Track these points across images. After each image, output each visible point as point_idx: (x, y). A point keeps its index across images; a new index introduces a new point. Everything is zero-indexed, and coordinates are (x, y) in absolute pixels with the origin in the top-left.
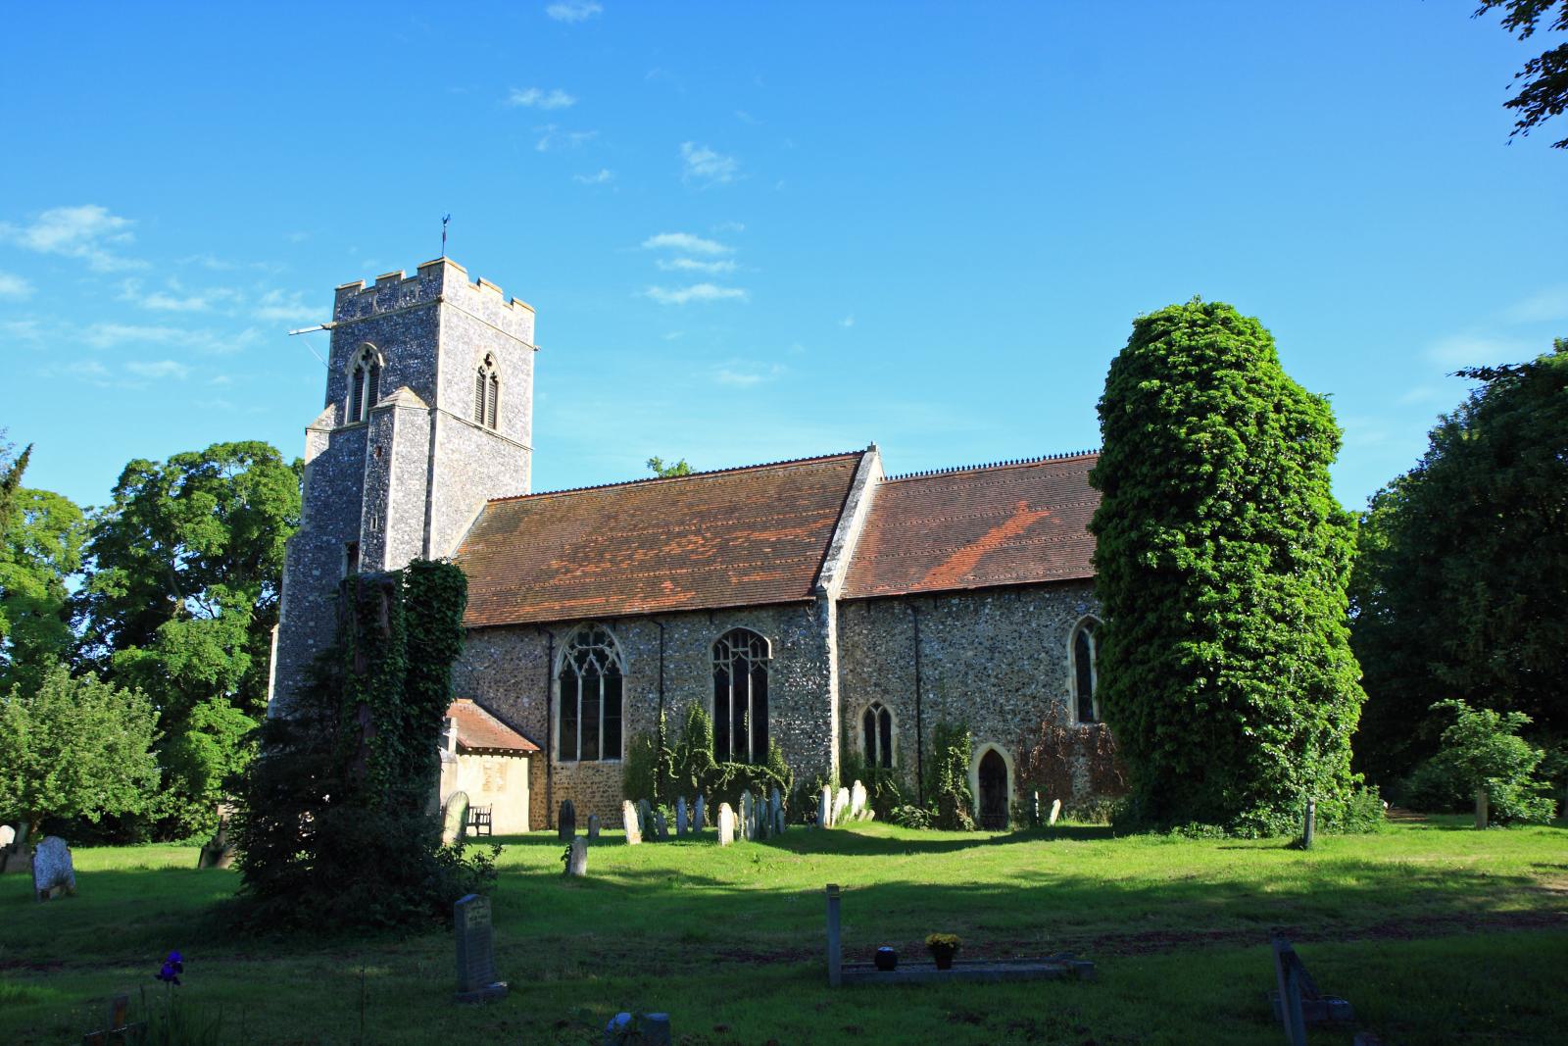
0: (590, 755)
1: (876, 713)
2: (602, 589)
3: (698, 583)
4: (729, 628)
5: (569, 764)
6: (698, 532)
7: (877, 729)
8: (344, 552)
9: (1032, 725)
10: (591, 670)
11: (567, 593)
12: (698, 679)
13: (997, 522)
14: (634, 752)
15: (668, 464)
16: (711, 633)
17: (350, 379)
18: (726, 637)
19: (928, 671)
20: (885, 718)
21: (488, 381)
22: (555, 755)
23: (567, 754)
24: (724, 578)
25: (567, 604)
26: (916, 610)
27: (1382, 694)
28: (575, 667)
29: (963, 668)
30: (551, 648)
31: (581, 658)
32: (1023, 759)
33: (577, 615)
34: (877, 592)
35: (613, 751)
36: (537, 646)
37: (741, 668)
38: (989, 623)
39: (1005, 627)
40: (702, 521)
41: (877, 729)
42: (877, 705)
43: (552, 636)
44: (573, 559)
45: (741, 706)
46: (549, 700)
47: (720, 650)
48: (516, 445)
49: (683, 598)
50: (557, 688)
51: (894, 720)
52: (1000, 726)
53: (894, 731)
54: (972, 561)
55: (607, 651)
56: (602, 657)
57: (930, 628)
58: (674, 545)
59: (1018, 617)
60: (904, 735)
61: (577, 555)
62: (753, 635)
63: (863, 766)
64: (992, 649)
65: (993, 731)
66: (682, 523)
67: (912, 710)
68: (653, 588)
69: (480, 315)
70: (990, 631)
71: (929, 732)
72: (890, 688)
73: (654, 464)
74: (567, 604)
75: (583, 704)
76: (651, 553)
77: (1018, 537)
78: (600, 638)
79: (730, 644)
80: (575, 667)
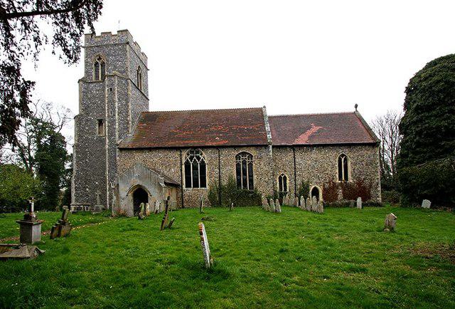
0: (196, 185)
5: (189, 189)
11: (179, 139)
12: (231, 166)
17: (278, 181)
19: (297, 166)
20: (285, 178)
22: (184, 186)
26: (294, 150)
30: (181, 155)
31: (191, 158)
32: (324, 190)
35: (203, 185)
36: (177, 154)
37: (244, 163)
38: (315, 154)
42: (283, 175)
43: (181, 152)
44: (180, 129)
45: (245, 181)
46: (181, 170)
50: (183, 167)
51: (288, 179)
53: (288, 182)
56: (199, 158)
57: (298, 155)
59: (323, 153)
60: (291, 183)
67: (293, 176)
68: (213, 139)
75: (190, 174)
77: (11, 271)
78: (198, 152)
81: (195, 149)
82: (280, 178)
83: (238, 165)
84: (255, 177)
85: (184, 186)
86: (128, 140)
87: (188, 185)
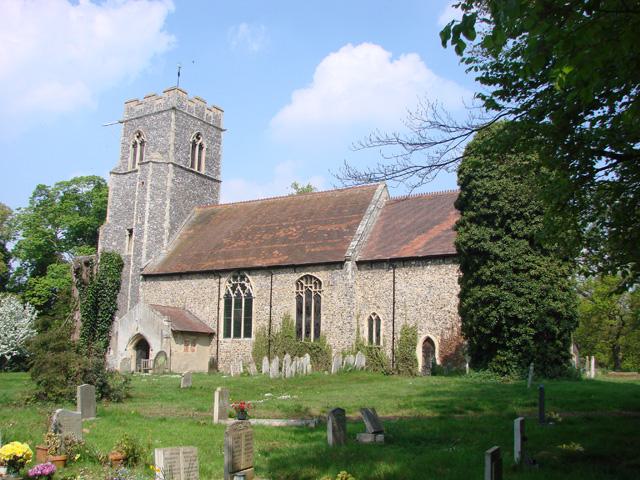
0: (237, 335)
1: (374, 318)
2: (245, 254)
3: (289, 251)
4: (304, 274)
6: (294, 225)
7: (374, 326)
8: (127, 233)
9: (448, 326)
10: (239, 294)
13: (437, 223)
14: (258, 335)
15: (302, 185)
16: (295, 277)
18: (302, 278)
20: (378, 320)
21: (197, 148)
23: (227, 335)
24: (302, 249)
25: (228, 261)
27: (139, 222)
28: (231, 292)
29: (416, 297)
33: (232, 267)
34: (375, 258)
35: (248, 334)
36: (210, 283)
37: (308, 293)
39: (437, 277)
40: (297, 220)
41: (374, 326)
45: (308, 314)
47: (298, 284)
48: (212, 179)
49: (282, 259)
50: (222, 302)
51: (382, 322)
52: (433, 326)
53: (382, 327)
54: (423, 243)
55: (246, 284)
56: (244, 287)
58: (281, 232)
61: (237, 237)
62: (315, 278)
63: (366, 344)
64: (430, 287)
65: (429, 329)
66: (287, 220)
69: (194, 115)
70: (430, 278)
71: (398, 329)
72: (381, 306)
73: (295, 186)
74: (228, 261)
76: (271, 236)
78: (243, 278)
79: (303, 282)
80: (231, 292)
81: (239, 273)
82: (370, 320)
83: (299, 298)
84: (323, 318)
85: (221, 335)
86: (152, 264)
87: (227, 335)
